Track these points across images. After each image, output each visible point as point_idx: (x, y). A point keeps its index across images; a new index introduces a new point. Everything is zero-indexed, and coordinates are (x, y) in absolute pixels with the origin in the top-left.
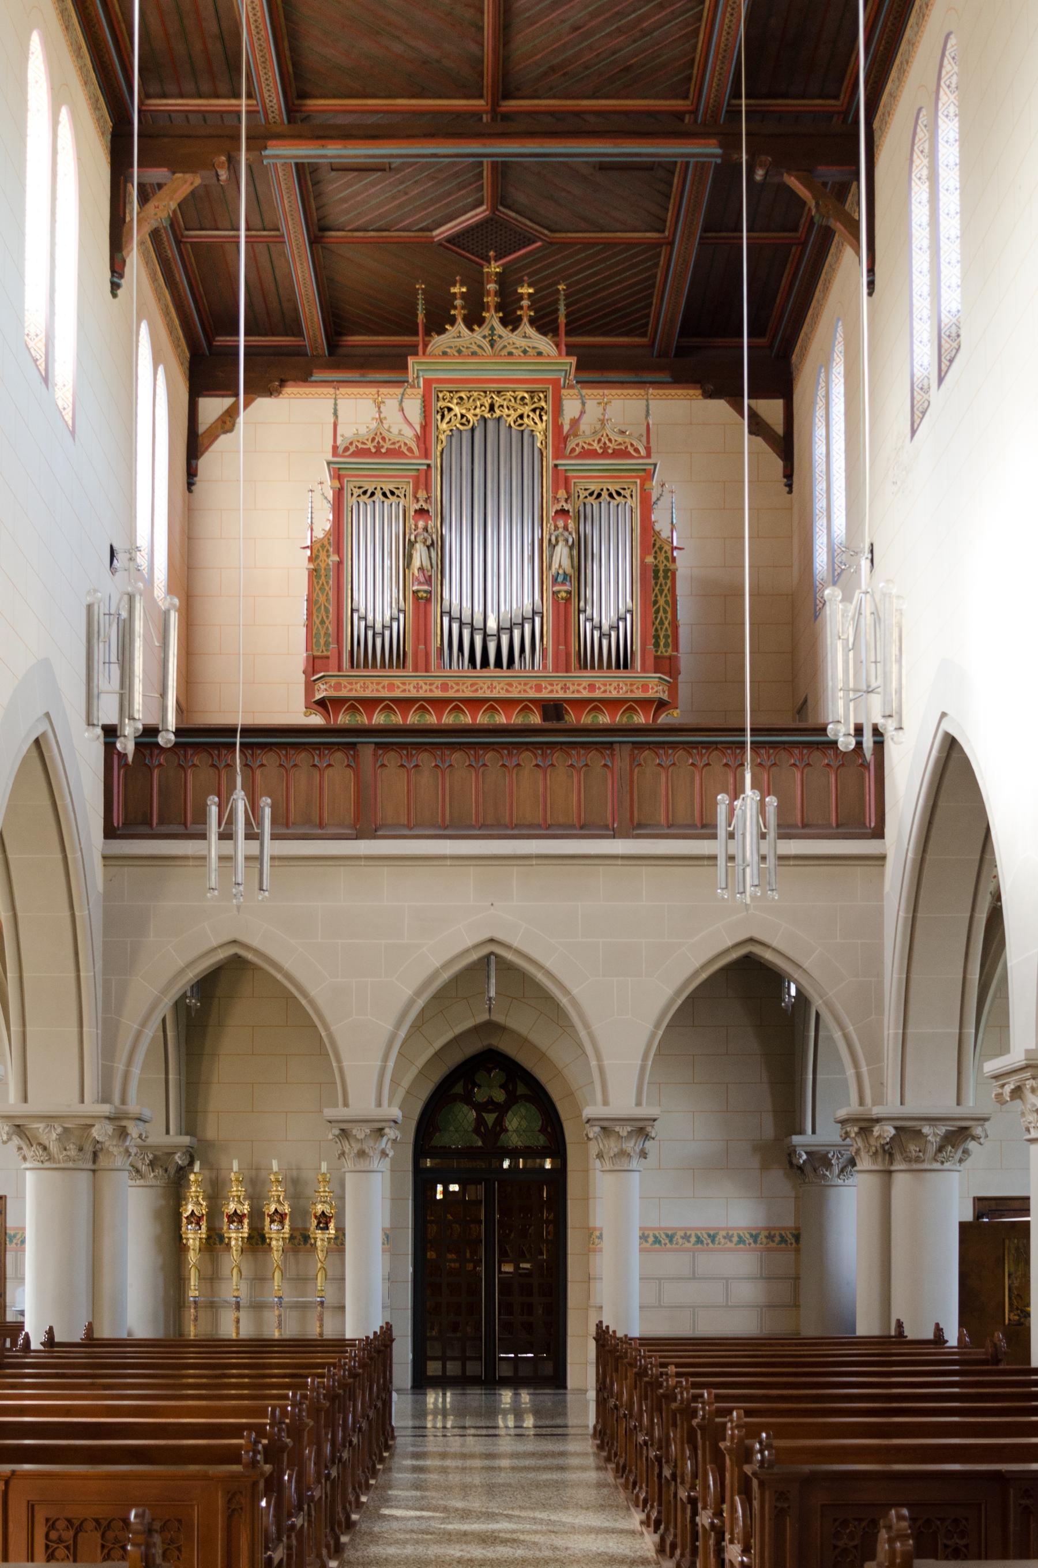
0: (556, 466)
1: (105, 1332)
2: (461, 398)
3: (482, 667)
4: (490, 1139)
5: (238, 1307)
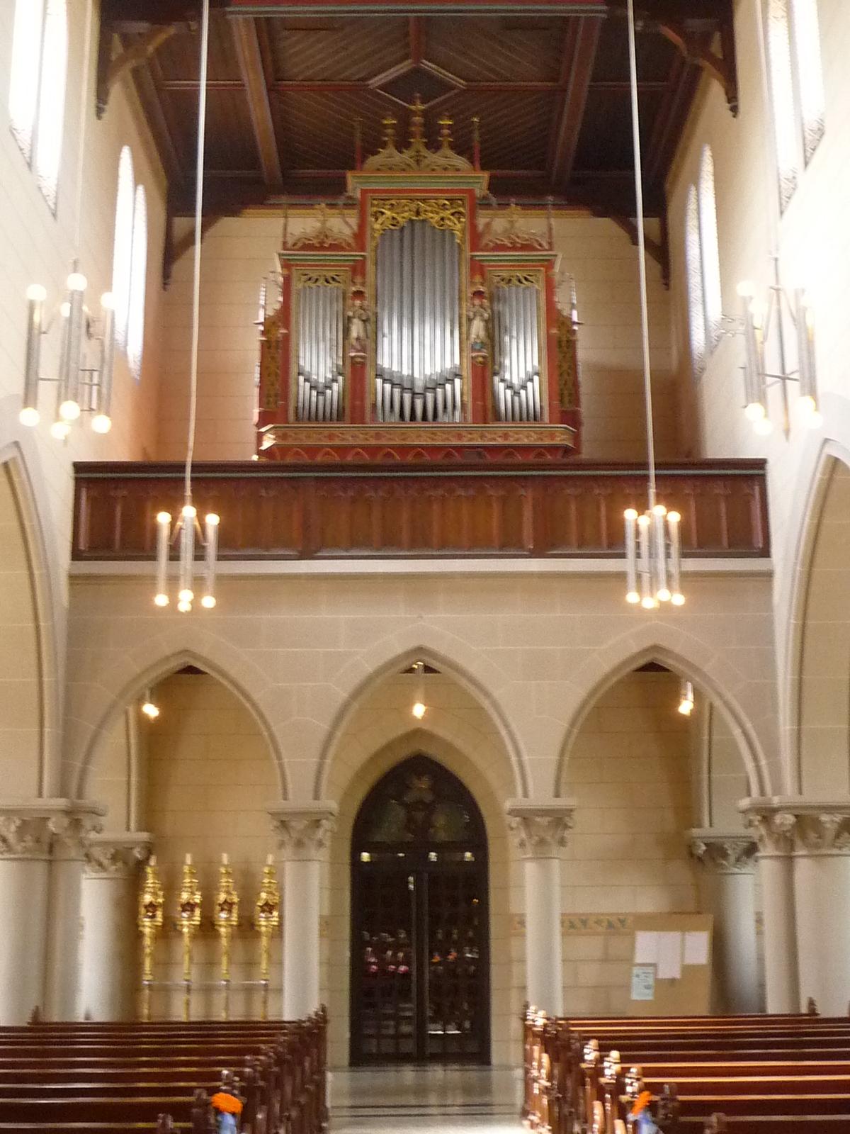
0: (472, 256)
1: (55, 1016)
2: (392, 205)
3: (411, 420)
4: (418, 865)
5: (189, 990)
